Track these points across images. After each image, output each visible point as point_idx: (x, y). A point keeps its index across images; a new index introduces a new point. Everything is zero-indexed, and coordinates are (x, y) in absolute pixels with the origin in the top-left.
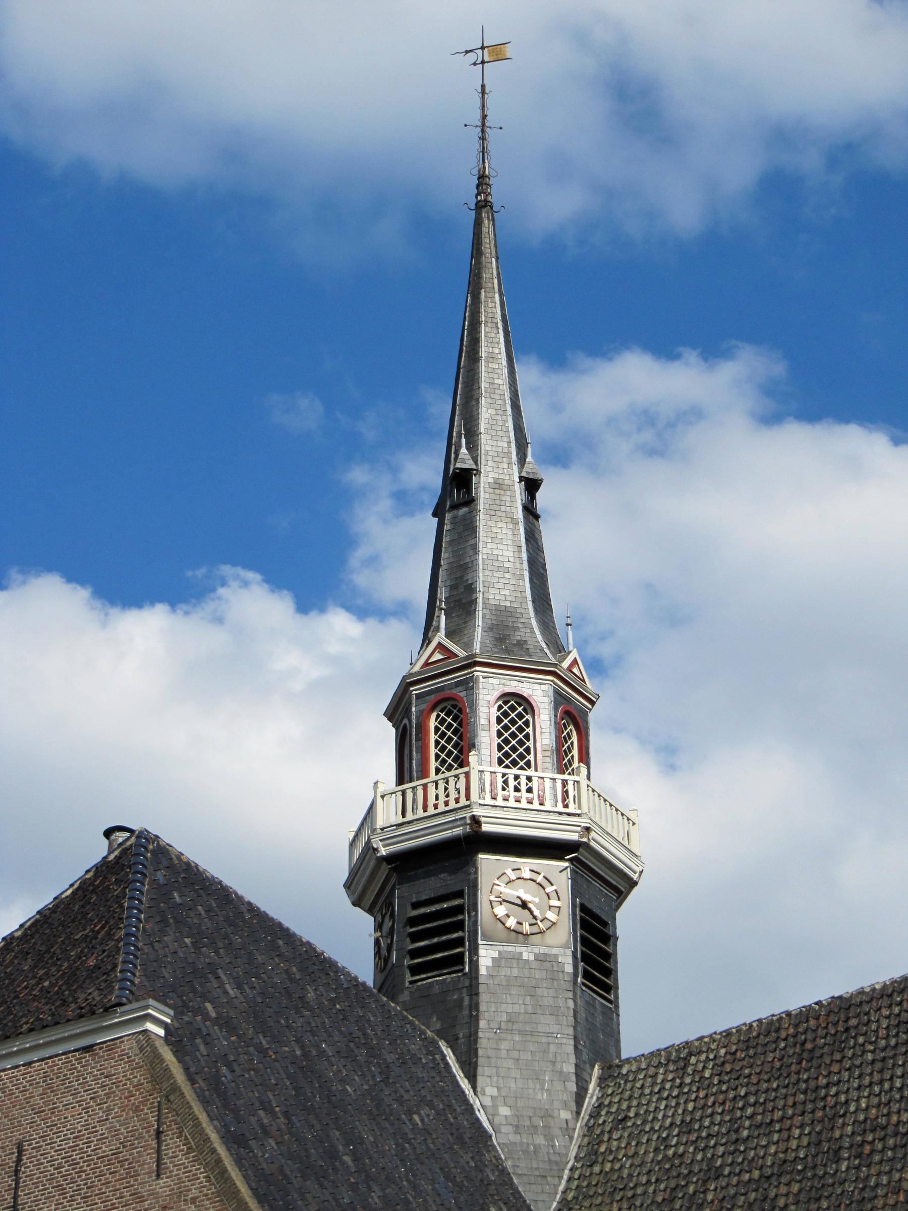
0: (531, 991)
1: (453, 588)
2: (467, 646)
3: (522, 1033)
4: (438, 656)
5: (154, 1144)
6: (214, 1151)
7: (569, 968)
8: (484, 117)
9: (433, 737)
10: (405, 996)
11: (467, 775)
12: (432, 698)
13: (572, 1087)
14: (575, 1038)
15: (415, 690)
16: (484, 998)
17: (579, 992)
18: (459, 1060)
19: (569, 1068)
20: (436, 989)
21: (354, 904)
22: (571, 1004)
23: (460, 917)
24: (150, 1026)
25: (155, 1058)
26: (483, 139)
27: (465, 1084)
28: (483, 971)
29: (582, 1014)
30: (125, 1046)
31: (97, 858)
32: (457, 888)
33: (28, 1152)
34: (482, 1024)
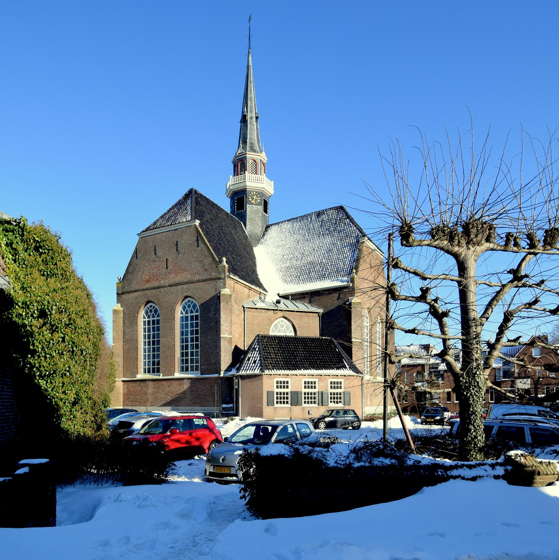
1: (243, 138)
8: (250, 35)
12: (240, 160)
20: (240, 213)
25: (198, 232)
26: (249, 39)
30: (193, 226)
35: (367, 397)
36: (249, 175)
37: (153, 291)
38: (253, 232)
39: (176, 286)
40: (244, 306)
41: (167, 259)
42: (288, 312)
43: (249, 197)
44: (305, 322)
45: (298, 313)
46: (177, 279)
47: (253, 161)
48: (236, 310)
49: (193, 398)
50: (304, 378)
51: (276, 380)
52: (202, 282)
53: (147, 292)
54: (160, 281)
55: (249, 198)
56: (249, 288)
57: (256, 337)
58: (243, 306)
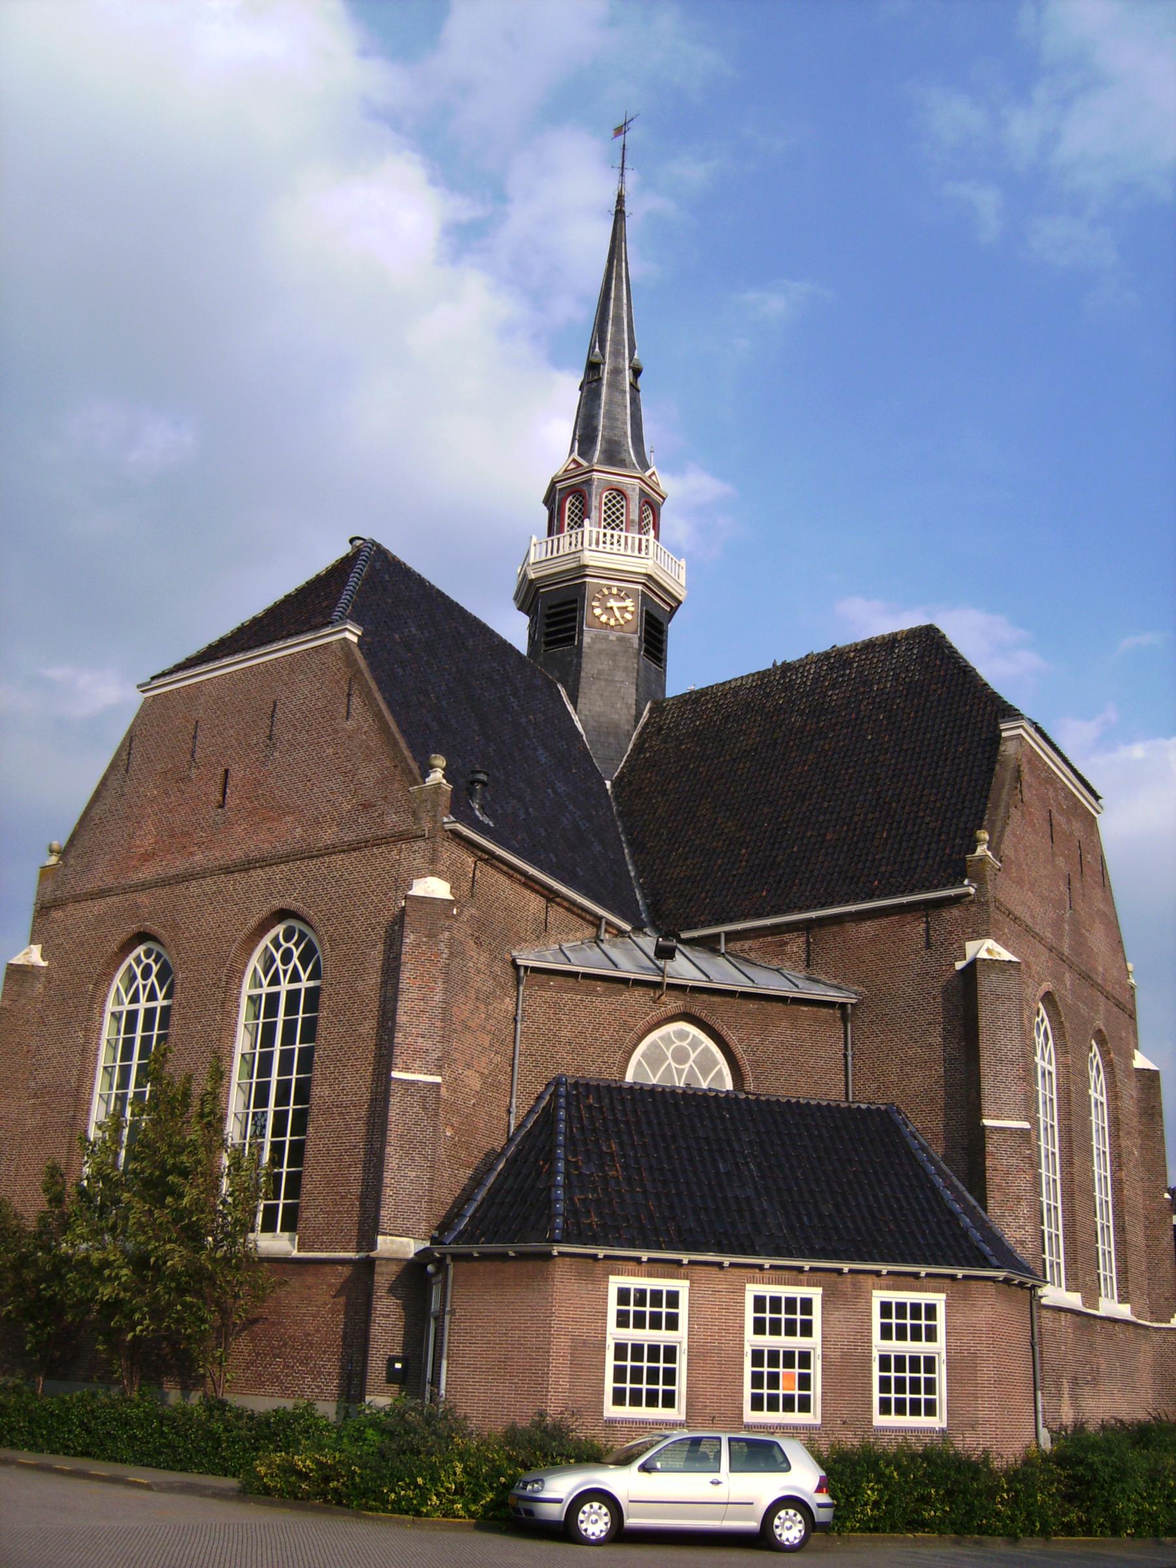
0: (613, 656)
2: (589, 461)
3: (606, 680)
4: (572, 466)
5: (346, 701)
6: (378, 705)
7: (636, 646)
9: (567, 513)
10: (541, 659)
11: (583, 532)
13: (633, 712)
14: (637, 685)
15: (559, 486)
16: (585, 660)
17: (641, 660)
18: (568, 694)
19: (632, 700)
21: (519, 609)
22: (636, 666)
23: (574, 614)
24: (348, 635)
27: (570, 708)
28: (584, 645)
29: (642, 673)
31: (343, 554)
32: (573, 598)
33: (279, 705)
34: (582, 674)
35: (1058, 1385)
36: (595, 530)
37: (162, 892)
38: (602, 719)
39: (247, 870)
40: (519, 962)
41: (227, 771)
42: (705, 997)
43: (594, 604)
44: (782, 1043)
45: (752, 1006)
46: (259, 843)
47: (614, 494)
48: (479, 971)
49: (258, 1354)
50: (753, 1281)
51: (615, 1282)
52: (344, 851)
53: (143, 898)
54: (192, 854)
55: (593, 608)
56: (546, 892)
57: (547, 1085)
58: (514, 961)
